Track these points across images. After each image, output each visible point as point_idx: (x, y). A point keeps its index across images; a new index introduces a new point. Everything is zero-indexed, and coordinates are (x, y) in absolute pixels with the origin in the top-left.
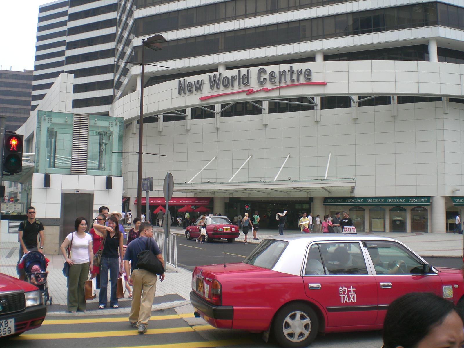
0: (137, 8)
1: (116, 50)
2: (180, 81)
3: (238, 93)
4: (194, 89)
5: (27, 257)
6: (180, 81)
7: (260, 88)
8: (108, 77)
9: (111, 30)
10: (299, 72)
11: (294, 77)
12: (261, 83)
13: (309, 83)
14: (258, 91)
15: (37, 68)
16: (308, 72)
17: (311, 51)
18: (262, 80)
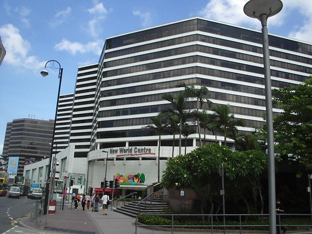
0: (100, 107)
1: (92, 126)
2: (111, 149)
3: (128, 155)
4: (115, 152)
5: (210, 102)
6: (111, 149)
7: (135, 154)
8: (88, 137)
9: (93, 99)
10: (147, 149)
11: (146, 151)
12: (136, 152)
13: (150, 153)
14: (134, 155)
15: (56, 120)
16: (150, 150)
17: (156, 140)
18: (136, 151)
